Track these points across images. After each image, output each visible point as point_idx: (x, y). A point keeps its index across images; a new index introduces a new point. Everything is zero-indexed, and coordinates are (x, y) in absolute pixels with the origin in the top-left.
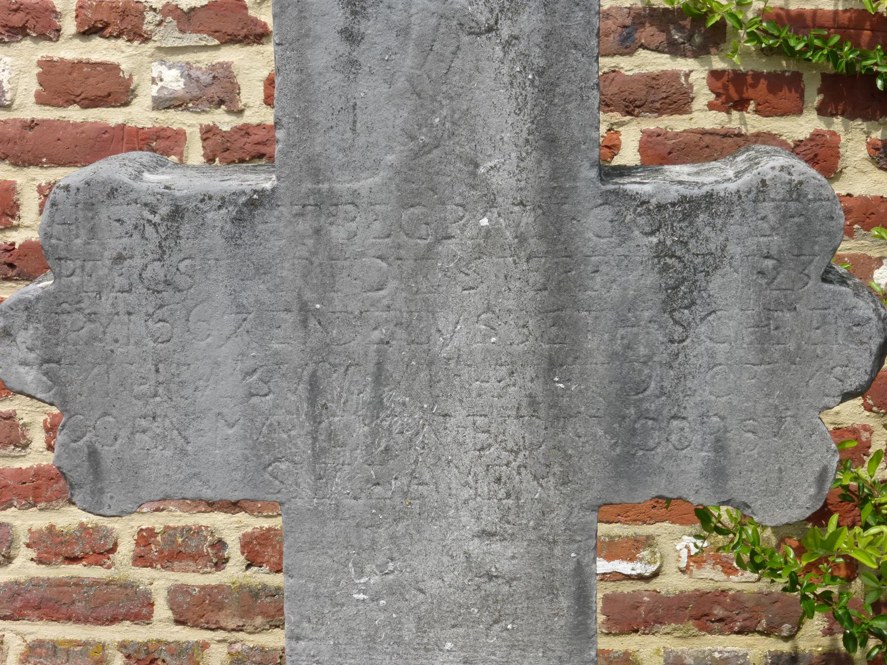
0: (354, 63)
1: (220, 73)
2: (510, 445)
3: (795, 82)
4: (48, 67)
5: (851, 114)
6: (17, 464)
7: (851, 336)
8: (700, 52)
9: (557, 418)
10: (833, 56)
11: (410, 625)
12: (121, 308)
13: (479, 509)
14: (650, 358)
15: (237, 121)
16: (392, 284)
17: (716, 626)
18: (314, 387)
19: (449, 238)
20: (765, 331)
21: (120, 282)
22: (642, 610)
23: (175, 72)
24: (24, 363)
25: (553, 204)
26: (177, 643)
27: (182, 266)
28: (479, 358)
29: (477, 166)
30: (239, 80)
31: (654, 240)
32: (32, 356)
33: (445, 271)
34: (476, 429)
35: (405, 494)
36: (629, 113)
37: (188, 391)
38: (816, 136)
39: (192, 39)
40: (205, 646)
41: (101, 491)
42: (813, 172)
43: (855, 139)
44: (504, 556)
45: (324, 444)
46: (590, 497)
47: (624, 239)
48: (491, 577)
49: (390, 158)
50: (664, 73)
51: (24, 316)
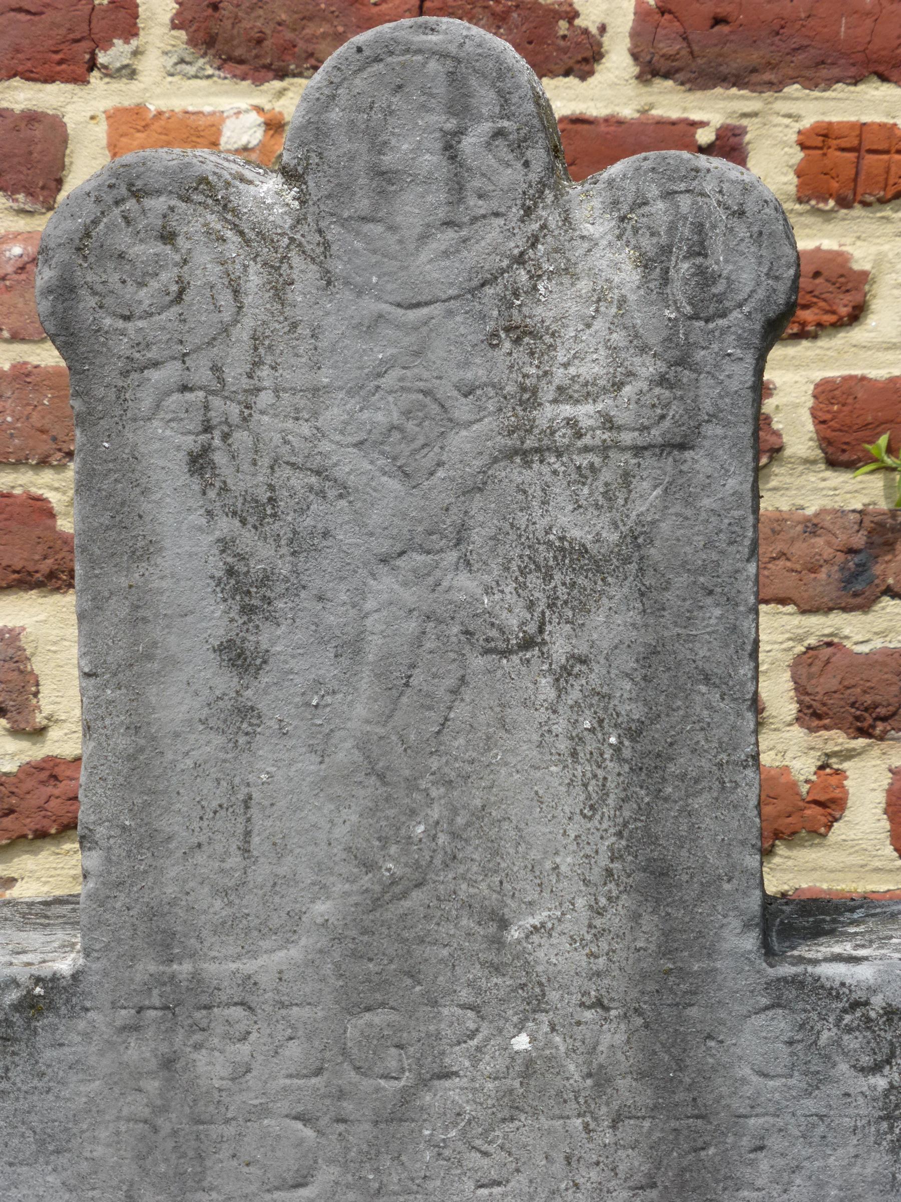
0: (245, 712)
16: (327, 1174)
25: (666, 1003)
29: (504, 924)
30: (37, 666)
31: (881, 1082)
33: (439, 1148)
47: (817, 1081)
49: (321, 908)
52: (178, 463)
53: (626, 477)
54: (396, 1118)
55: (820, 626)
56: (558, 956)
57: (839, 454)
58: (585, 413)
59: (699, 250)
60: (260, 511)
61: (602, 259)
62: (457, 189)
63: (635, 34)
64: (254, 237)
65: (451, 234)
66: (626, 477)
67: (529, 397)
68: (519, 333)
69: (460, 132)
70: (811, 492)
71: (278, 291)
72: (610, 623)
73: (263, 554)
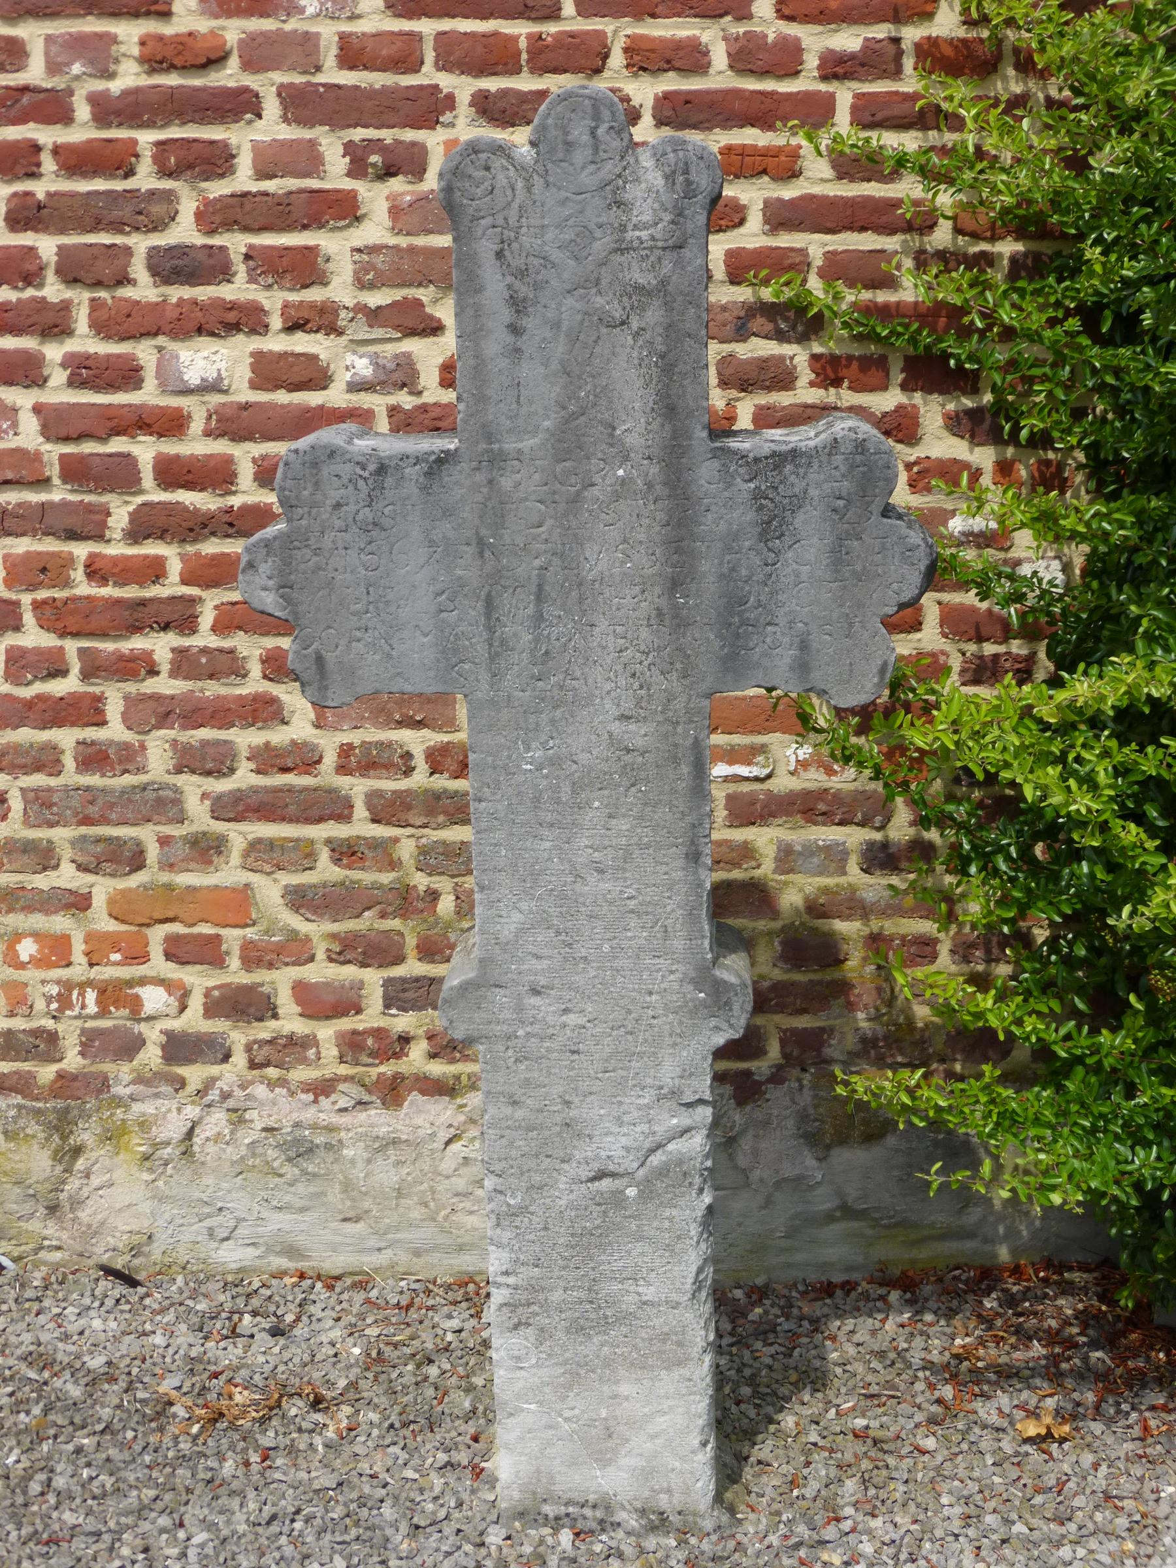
0: (518, 350)
1: (402, 361)
2: (643, 647)
3: (881, 363)
4: (259, 357)
5: (928, 390)
6: (238, 691)
7: (904, 559)
8: (802, 339)
9: (679, 626)
10: (913, 341)
11: (566, 789)
12: (340, 544)
13: (619, 698)
14: (750, 578)
15: (418, 401)
16: (550, 522)
17: (820, 818)
18: (490, 605)
19: (593, 485)
20: (838, 556)
21: (339, 523)
22: (758, 806)
23: (365, 361)
24: (265, 589)
25: (674, 457)
26: (374, 838)
27: (386, 511)
28: (618, 579)
29: (614, 429)
30: (418, 366)
31: (752, 485)
32: (271, 583)
33: (590, 512)
34: (616, 635)
35: (561, 687)
36: (744, 390)
37: (392, 609)
38: (900, 408)
39: (379, 333)
40: (396, 840)
41: (326, 688)
42: (875, 432)
43: (933, 411)
44: (638, 734)
45: (498, 648)
46: (704, 687)
47: (729, 485)
48: (628, 751)
49: (547, 423)
50: (773, 356)
51: (264, 551)
52: (491, 255)
53: (660, 259)
54: (574, 501)
55: (727, 348)
56: (634, 440)
57: (735, 279)
58: (644, 234)
59: (686, 172)
60: (522, 274)
61: (650, 176)
62: (596, 149)
63: (654, 108)
64: (520, 168)
65: (593, 166)
66: (660, 259)
67: (623, 228)
68: (619, 204)
69: (596, 127)
70: (725, 294)
71: (529, 189)
72: (654, 315)
73: (524, 290)
